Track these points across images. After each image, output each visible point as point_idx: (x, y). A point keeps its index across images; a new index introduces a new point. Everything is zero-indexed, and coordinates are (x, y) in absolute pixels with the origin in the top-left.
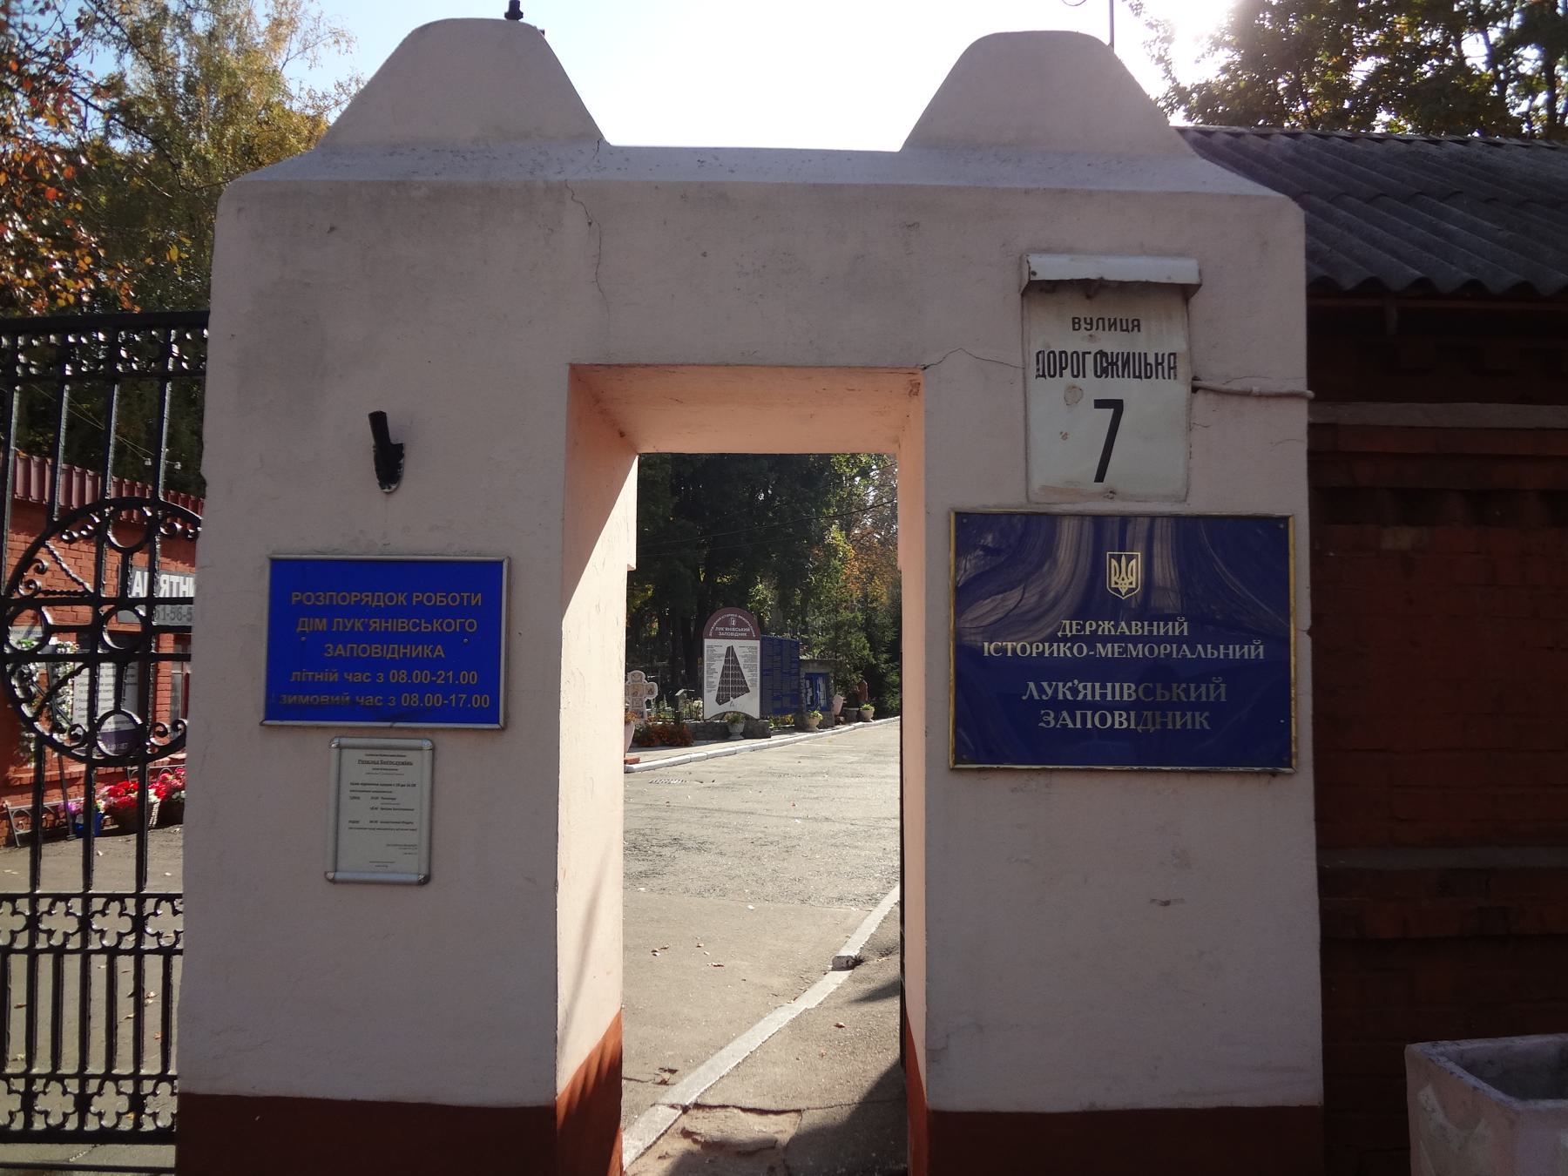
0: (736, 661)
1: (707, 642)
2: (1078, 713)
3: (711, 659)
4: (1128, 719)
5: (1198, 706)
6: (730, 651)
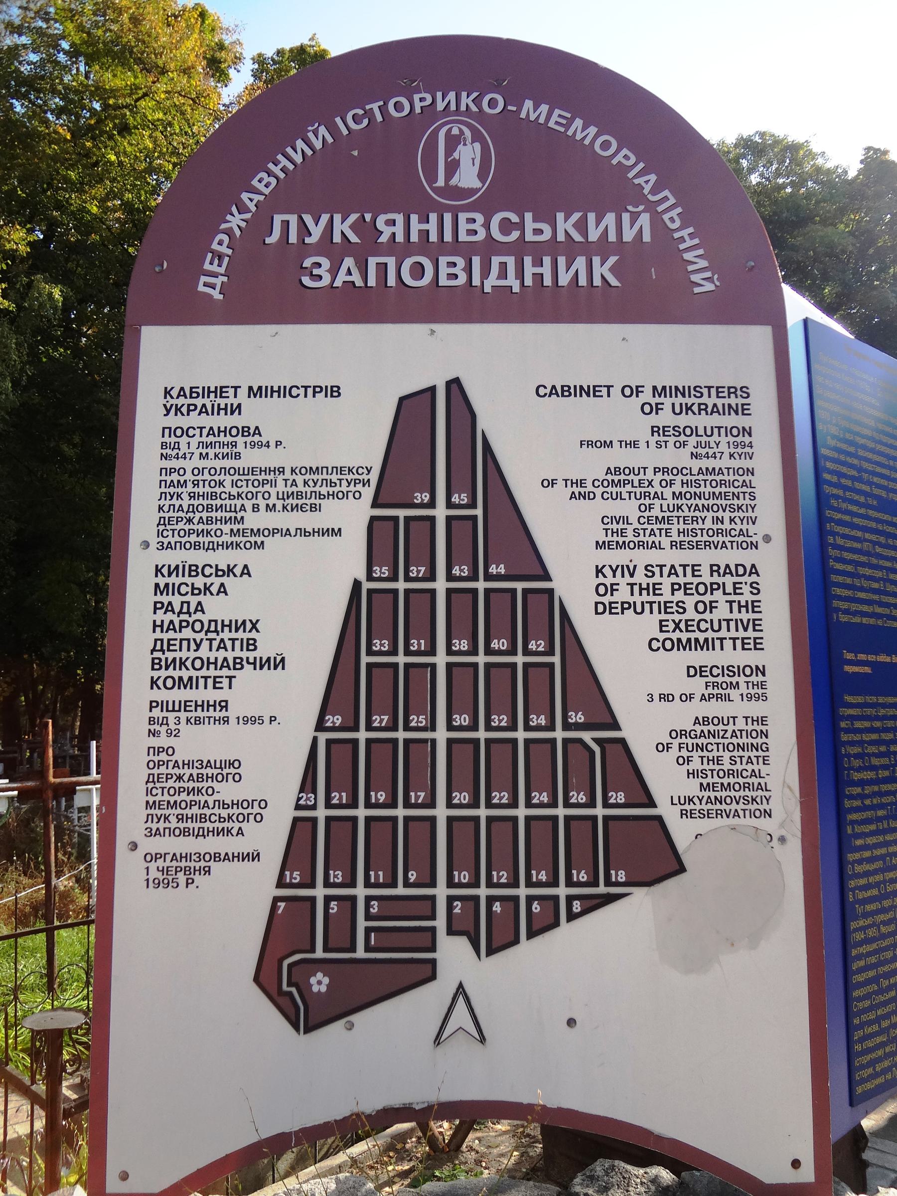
0: (500, 530)
1: (167, 358)
2: (372, 262)
3: (208, 515)
4: (469, 270)
5: (603, 248)
6: (435, 435)
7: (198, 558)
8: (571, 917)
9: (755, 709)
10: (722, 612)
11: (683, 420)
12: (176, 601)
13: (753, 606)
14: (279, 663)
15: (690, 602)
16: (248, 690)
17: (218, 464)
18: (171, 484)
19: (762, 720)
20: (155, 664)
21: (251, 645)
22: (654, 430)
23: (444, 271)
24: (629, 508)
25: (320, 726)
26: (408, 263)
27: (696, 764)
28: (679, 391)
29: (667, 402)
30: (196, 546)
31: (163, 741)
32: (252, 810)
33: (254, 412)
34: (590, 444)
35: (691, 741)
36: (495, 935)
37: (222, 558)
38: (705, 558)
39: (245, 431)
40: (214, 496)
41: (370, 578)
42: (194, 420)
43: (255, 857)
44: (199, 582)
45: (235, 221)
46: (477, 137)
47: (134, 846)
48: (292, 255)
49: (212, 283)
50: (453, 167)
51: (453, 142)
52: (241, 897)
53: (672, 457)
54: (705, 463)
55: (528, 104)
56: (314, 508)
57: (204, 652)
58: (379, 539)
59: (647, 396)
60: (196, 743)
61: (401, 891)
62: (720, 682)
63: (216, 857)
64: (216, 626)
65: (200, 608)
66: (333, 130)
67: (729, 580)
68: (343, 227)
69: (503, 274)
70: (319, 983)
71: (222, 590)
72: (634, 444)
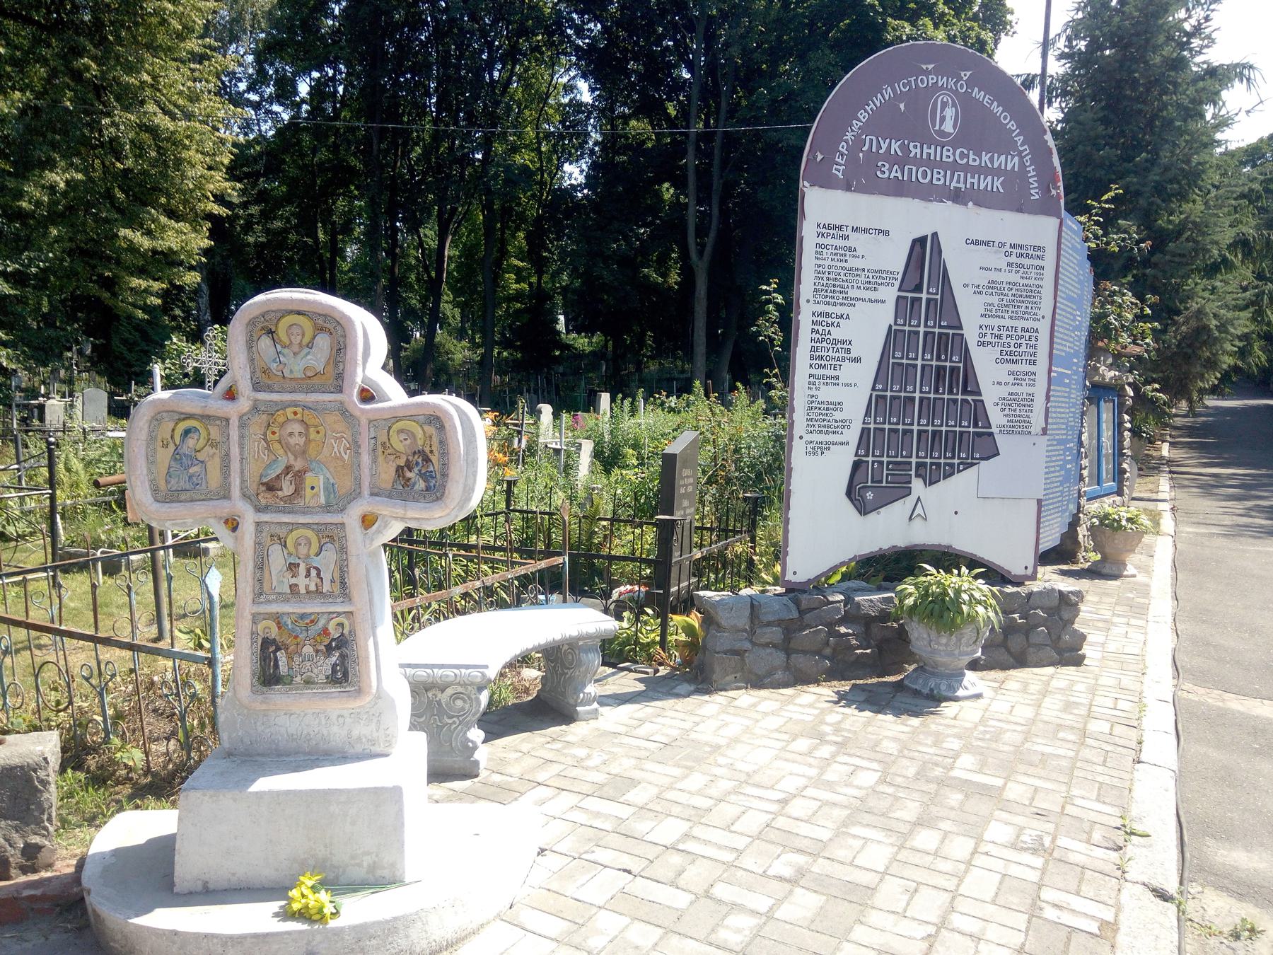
0: (945, 306)
3: (832, 289)
6: (923, 251)
7: (830, 309)
8: (959, 471)
9: (1031, 390)
10: (1023, 348)
11: (1019, 261)
12: (820, 328)
13: (1035, 346)
14: (859, 360)
15: (1012, 343)
16: (847, 372)
17: (839, 264)
18: (819, 273)
19: (1032, 395)
20: (812, 357)
21: (848, 351)
22: (1008, 264)
23: (935, 176)
24: (994, 300)
25: (873, 389)
26: (921, 170)
27: (1007, 412)
28: (1020, 247)
29: (1015, 251)
30: (829, 303)
31: (814, 392)
32: (846, 423)
33: (856, 240)
34: (976, 243)
35: (1008, 401)
36: (932, 476)
37: (839, 310)
38: (1020, 324)
39: (850, 249)
40: (836, 280)
41: (896, 324)
42: (829, 241)
43: (847, 444)
44: (830, 321)
45: (849, 136)
46: (954, 105)
47: (801, 438)
48: (872, 157)
49: (838, 171)
50: (943, 119)
51: (944, 105)
52: (841, 461)
53: (1014, 277)
54: (1026, 281)
55: (976, 89)
56: (876, 289)
57: (830, 353)
58: (905, 307)
59: (1007, 248)
60: (827, 394)
61: (899, 459)
62: (1019, 377)
63: (833, 443)
64: (835, 342)
65: (829, 333)
66: (894, 90)
67: (1028, 334)
68: (895, 146)
69: (958, 182)
70: (870, 495)
71: (838, 325)
72: (1000, 270)
